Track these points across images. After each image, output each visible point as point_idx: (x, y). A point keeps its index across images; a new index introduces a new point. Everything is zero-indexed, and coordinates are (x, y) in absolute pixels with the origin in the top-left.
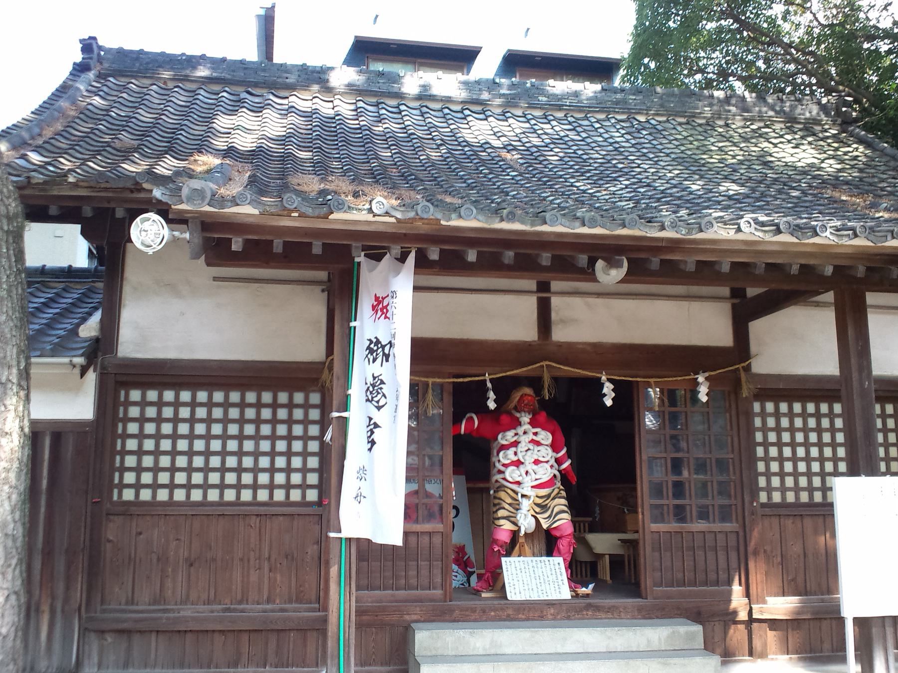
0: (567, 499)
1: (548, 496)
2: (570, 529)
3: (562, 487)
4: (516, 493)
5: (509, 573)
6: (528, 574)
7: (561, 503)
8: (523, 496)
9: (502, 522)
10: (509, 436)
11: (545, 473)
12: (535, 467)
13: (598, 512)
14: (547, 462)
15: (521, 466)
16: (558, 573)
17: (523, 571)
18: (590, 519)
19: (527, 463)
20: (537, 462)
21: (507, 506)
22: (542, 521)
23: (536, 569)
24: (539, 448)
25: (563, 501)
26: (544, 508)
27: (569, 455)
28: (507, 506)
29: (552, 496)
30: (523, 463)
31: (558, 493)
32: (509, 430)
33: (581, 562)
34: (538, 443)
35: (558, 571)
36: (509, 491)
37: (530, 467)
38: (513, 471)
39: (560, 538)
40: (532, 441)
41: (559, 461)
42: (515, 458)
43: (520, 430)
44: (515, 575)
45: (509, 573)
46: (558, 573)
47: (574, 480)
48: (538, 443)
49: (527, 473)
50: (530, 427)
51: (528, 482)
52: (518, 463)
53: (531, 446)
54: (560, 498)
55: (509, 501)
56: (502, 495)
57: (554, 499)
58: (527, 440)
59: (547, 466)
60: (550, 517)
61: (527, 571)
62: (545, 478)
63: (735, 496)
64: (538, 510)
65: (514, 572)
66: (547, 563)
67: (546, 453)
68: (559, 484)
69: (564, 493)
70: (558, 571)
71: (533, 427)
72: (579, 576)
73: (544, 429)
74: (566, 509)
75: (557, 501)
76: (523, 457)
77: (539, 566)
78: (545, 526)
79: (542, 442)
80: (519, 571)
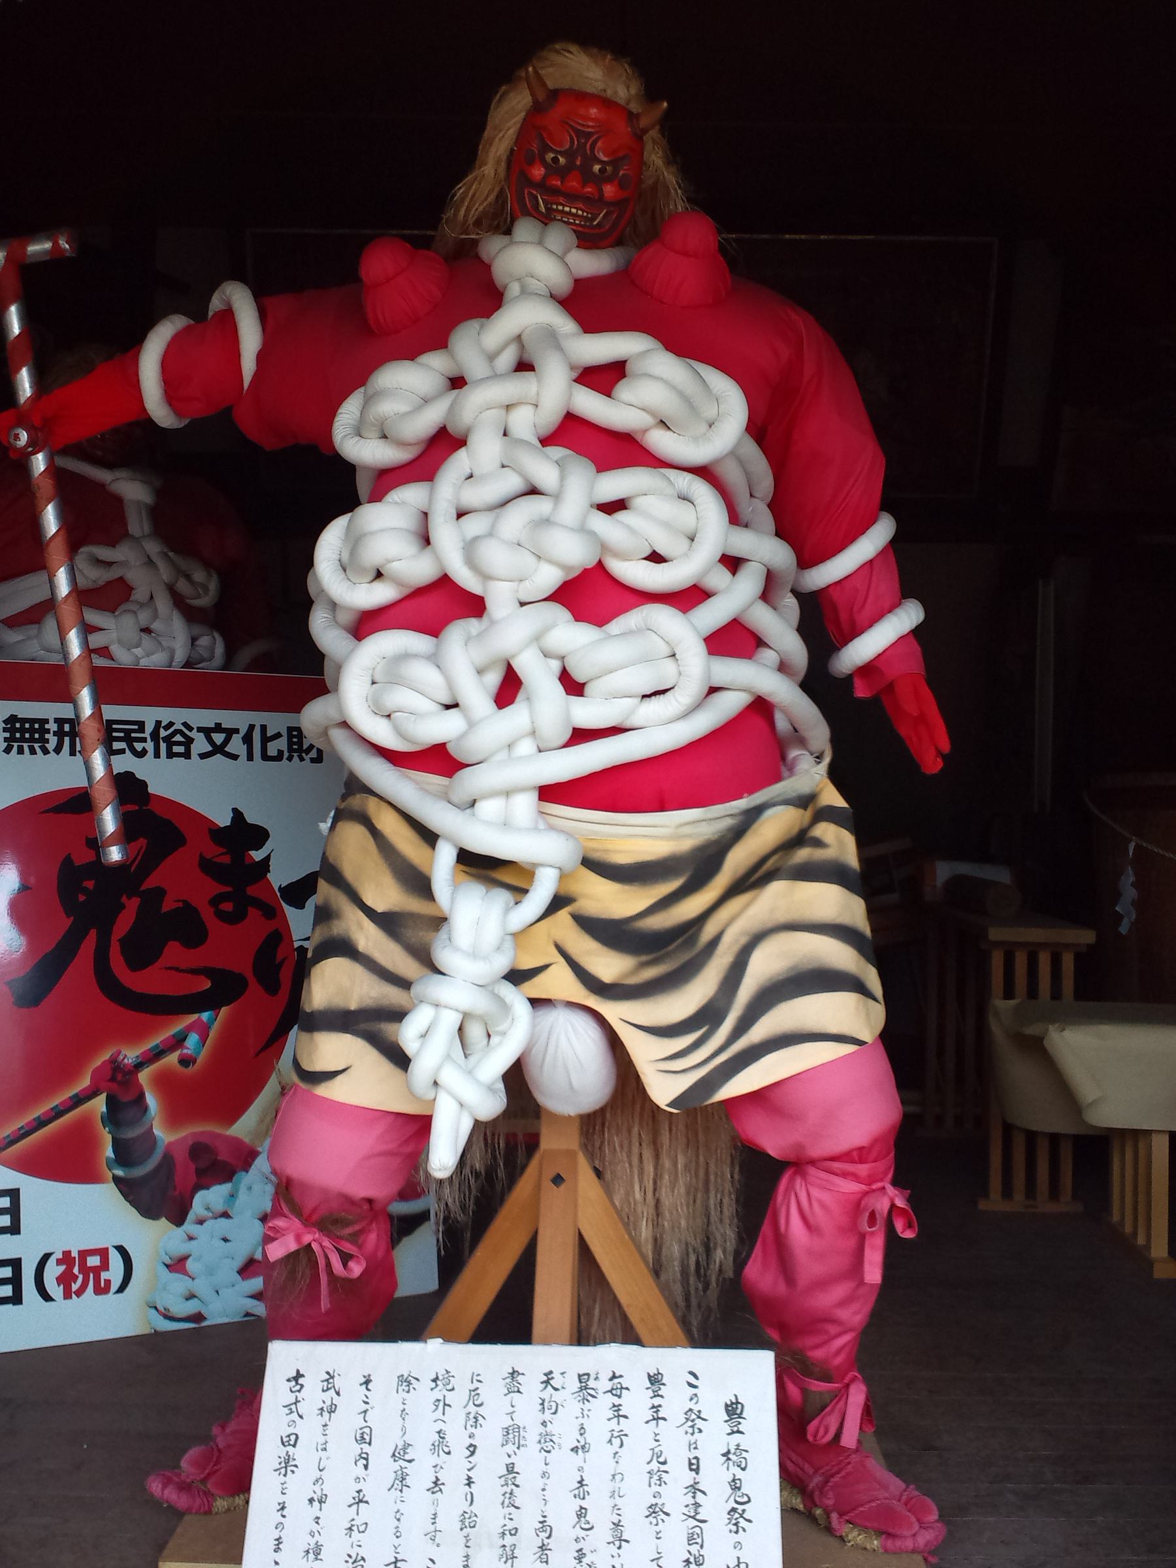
0: (864, 881)
1: (701, 864)
2: (865, 1112)
3: (833, 797)
4: (429, 837)
5: (300, 1485)
6: (452, 1502)
7: (808, 918)
8: (475, 864)
9: (330, 1049)
10: (395, 402)
11: (658, 685)
12: (571, 635)
13: (1129, 892)
14: (689, 598)
15: (458, 632)
16: (715, 1506)
17: (420, 1476)
18: (1087, 937)
19: (499, 599)
20: (591, 594)
21: (368, 937)
22: (646, 1053)
23: (529, 1461)
24: (614, 484)
25: (848, 907)
26: (665, 952)
27: (907, 570)
28: (368, 937)
29: (738, 859)
30: (475, 606)
31: (800, 839)
32: (411, 353)
33: (1031, 1137)
34: (618, 449)
35: (715, 1476)
36: (389, 824)
37: (525, 630)
38: (391, 674)
39: (798, 1164)
40: (570, 432)
41: (825, 621)
42: (418, 569)
43: (478, 344)
44: (337, 1513)
45: (300, 1485)
46: (715, 1506)
47: (931, 746)
48: (618, 449)
49: (509, 688)
50: (565, 324)
51: (517, 753)
52: (441, 605)
53: (544, 468)
54: (807, 873)
55: (384, 893)
56: (352, 848)
57: (753, 880)
58: (525, 423)
59: (684, 631)
60: (707, 1017)
61: (454, 1469)
62: (661, 731)
63: (581, 736)
64: (610, 965)
65: (341, 1481)
66: (637, 1401)
67: (675, 527)
68: (810, 774)
69: (840, 844)
70: (715, 1476)
71: (591, 323)
72: (1019, 1196)
73: (680, 345)
74: (840, 955)
75: (780, 898)
76: (469, 548)
77: (565, 1428)
78: (664, 1089)
79: (661, 442)
80: (383, 1466)
